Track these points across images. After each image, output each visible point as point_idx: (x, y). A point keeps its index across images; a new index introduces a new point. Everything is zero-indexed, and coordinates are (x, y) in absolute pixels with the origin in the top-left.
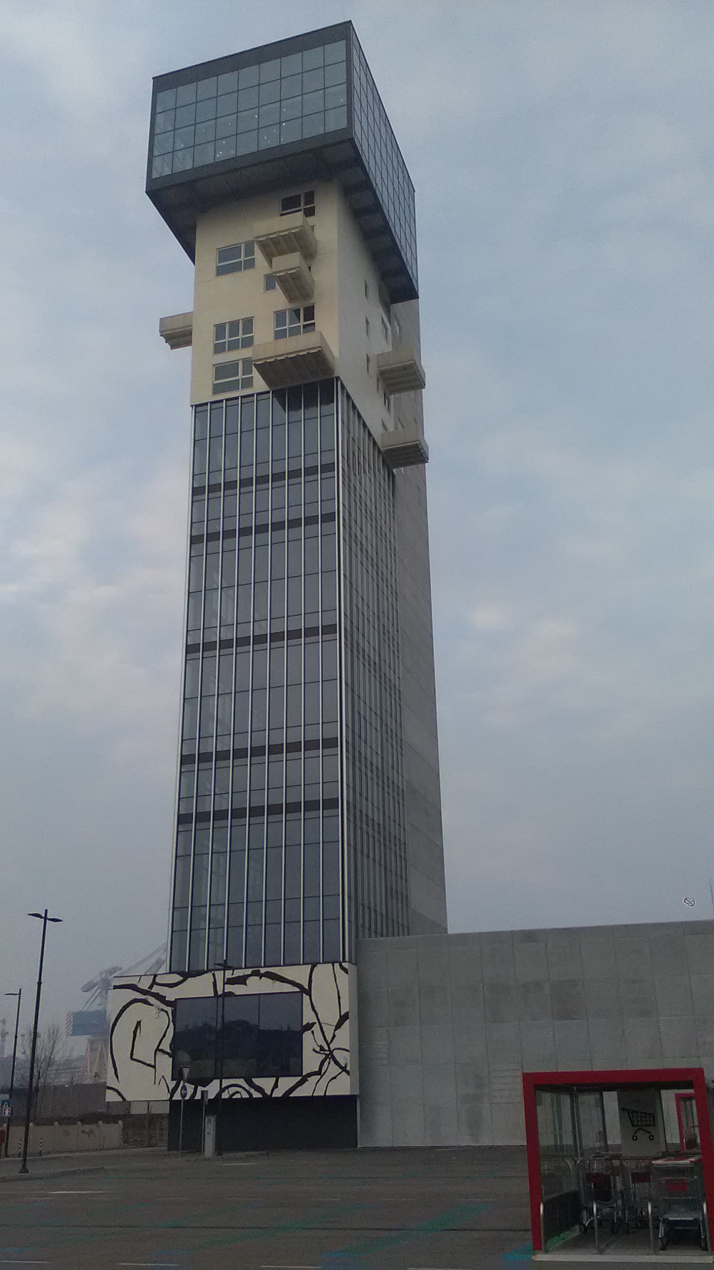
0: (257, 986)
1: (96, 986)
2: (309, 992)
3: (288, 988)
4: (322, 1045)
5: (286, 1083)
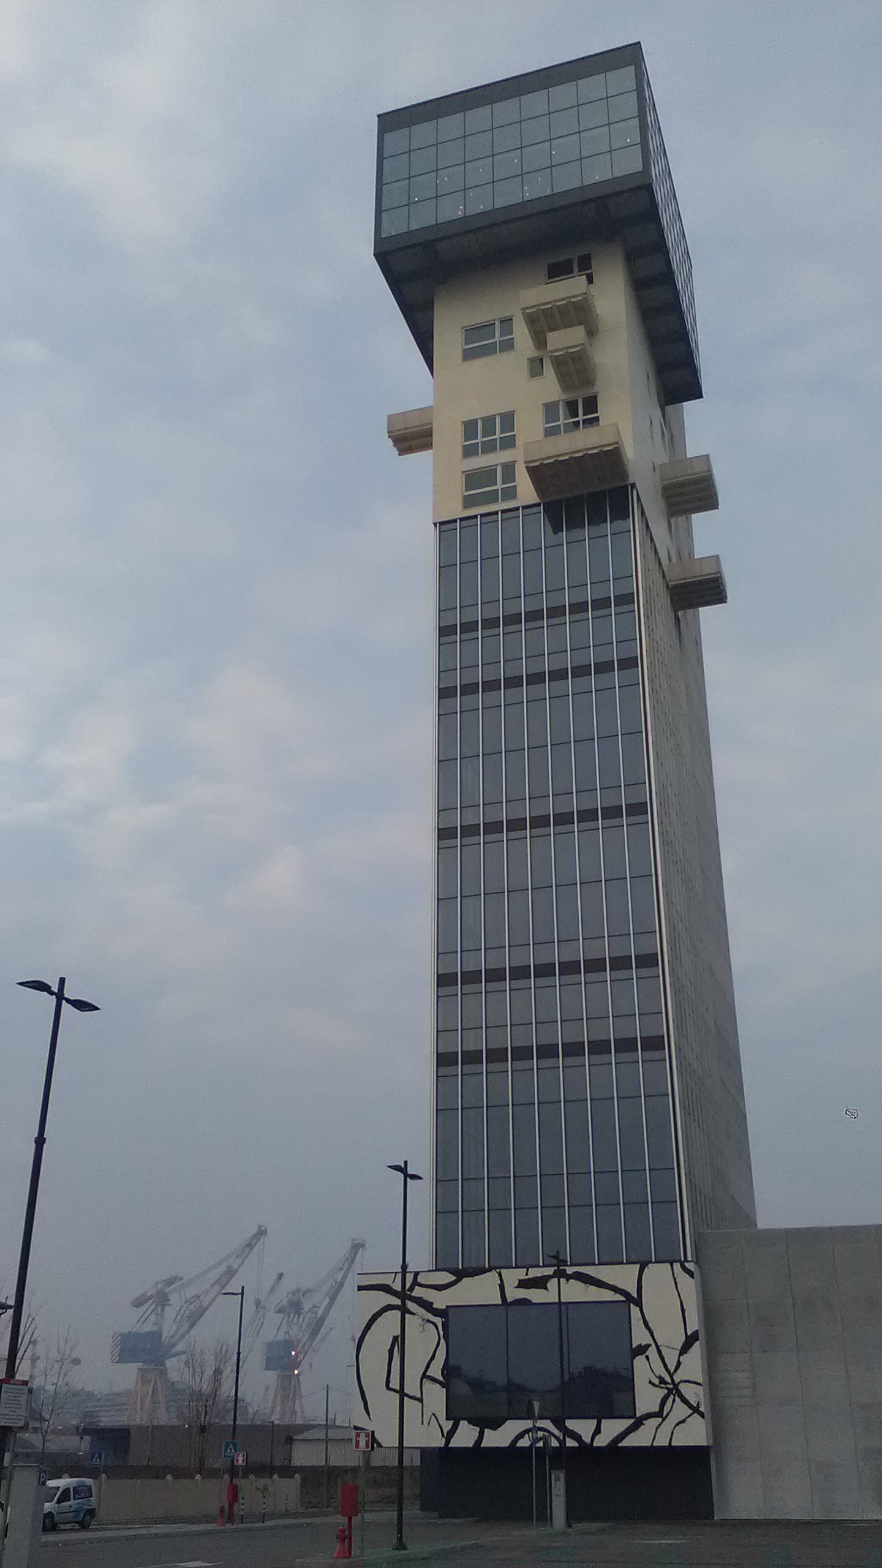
0: (574, 1292)
1: (150, 1299)
2: (639, 1302)
3: (608, 1295)
4: (663, 1376)
5: (612, 1428)
